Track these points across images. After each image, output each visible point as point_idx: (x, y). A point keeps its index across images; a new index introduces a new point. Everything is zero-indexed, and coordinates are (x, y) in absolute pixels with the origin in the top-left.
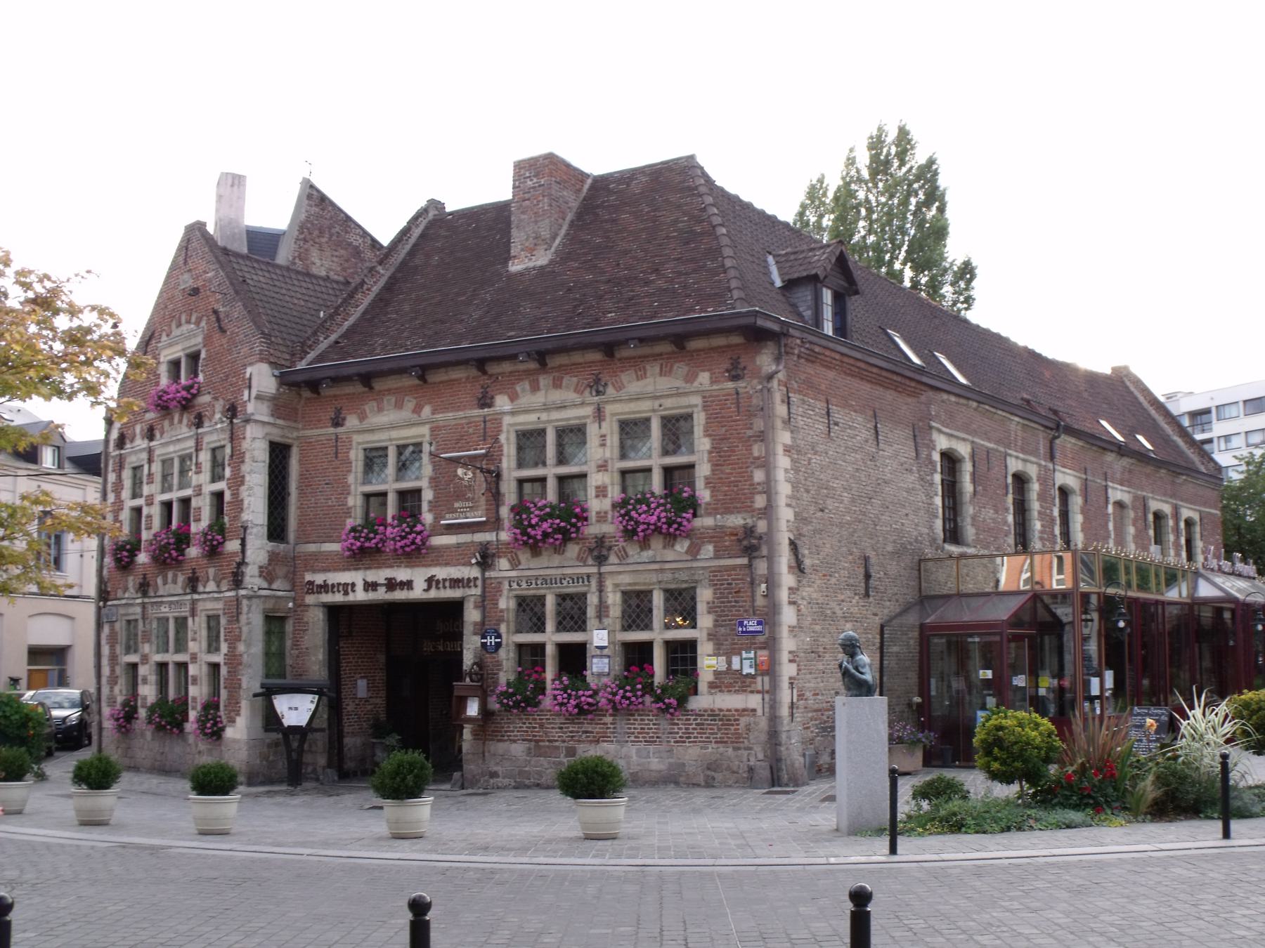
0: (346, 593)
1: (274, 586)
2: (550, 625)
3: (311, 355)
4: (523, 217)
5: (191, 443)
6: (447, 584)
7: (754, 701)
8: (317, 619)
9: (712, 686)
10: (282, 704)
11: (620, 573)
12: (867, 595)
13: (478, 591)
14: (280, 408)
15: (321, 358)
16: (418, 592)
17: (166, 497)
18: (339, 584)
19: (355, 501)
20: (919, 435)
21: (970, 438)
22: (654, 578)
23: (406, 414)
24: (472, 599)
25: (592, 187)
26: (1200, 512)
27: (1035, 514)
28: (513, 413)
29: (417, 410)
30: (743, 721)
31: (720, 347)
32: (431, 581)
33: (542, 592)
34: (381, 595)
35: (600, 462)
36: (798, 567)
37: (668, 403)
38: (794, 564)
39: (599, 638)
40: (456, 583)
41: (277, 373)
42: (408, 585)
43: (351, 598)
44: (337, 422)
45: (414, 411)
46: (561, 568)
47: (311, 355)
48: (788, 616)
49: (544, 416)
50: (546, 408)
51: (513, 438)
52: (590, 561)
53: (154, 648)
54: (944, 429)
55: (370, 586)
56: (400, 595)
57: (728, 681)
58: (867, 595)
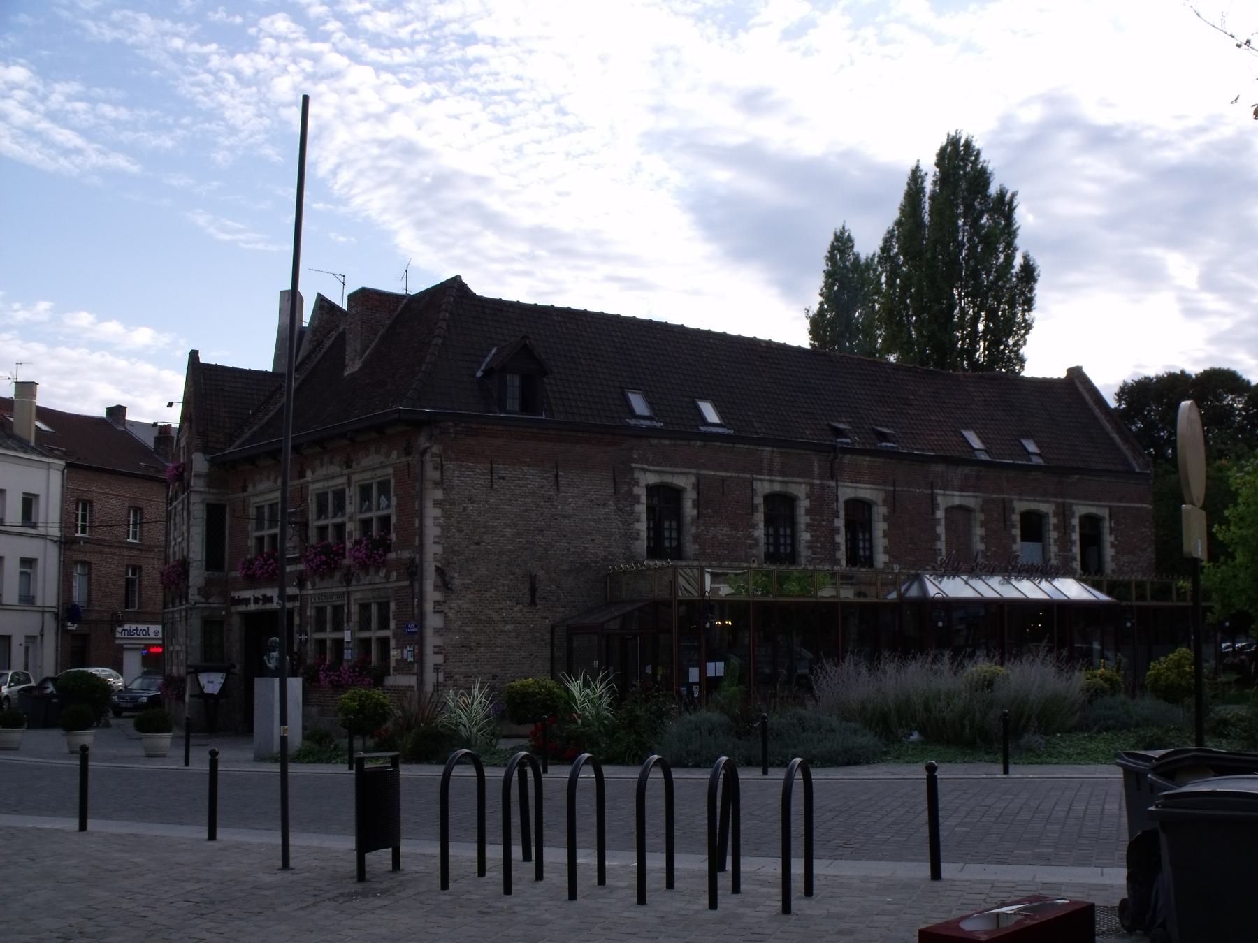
1: (211, 600)
3: (237, 443)
5: (344, 480)
7: (412, 681)
8: (236, 621)
9: (395, 669)
10: (204, 679)
12: (533, 603)
13: (298, 604)
14: (213, 480)
15: (243, 444)
17: (322, 523)
19: (251, 543)
20: (621, 476)
21: (694, 471)
25: (406, 306)
26: (1110, 508)
27: (803, 527)
30: (409, 693)
36: (444, 584)
37: (379, 472)
38: (440, 583)
39: (347, 635)
41: (208, 457)
44: (244, 489)
46: (332, 587)
47: (237, 443)
48: (433, 621)
49: (326, 484)
50: (327, 478)
51: (314, 498)
54: (652, 468)
57: (404, 668)
58: (533, 603)
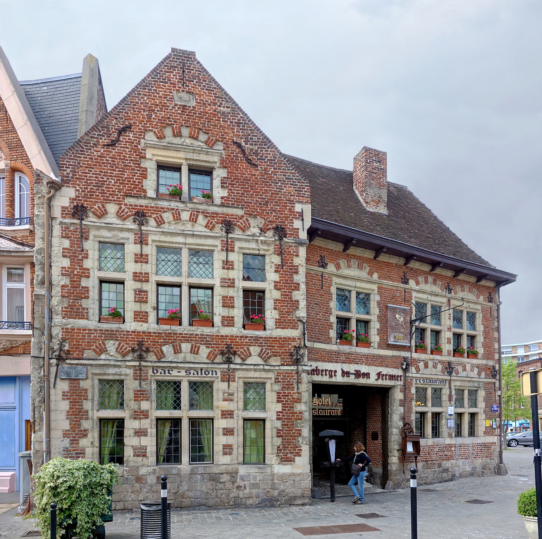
0: (331, 376)
2: (429, 404)
4: (372, 182)
6: (388, 377)
11: (457, 380)
13: (402, 383)
16: (372, 381)
18: (326, 370)
22: (467, 384)
23: (363, 274)
24: (399, 387)
28: (418, 291)
29: (370, 274)
30: (493, 447)
31: (488, 287)
32: (379, 375)
33: (427, 386)
34: (352, 380)
35: (449, 327)
40: (392, 377)
42: (367, 375)
43: (333, 379)
45: (368, 274)
52: (446, 374)
53: (154, 405)
55: (345, 374)
56: (362, 381)
